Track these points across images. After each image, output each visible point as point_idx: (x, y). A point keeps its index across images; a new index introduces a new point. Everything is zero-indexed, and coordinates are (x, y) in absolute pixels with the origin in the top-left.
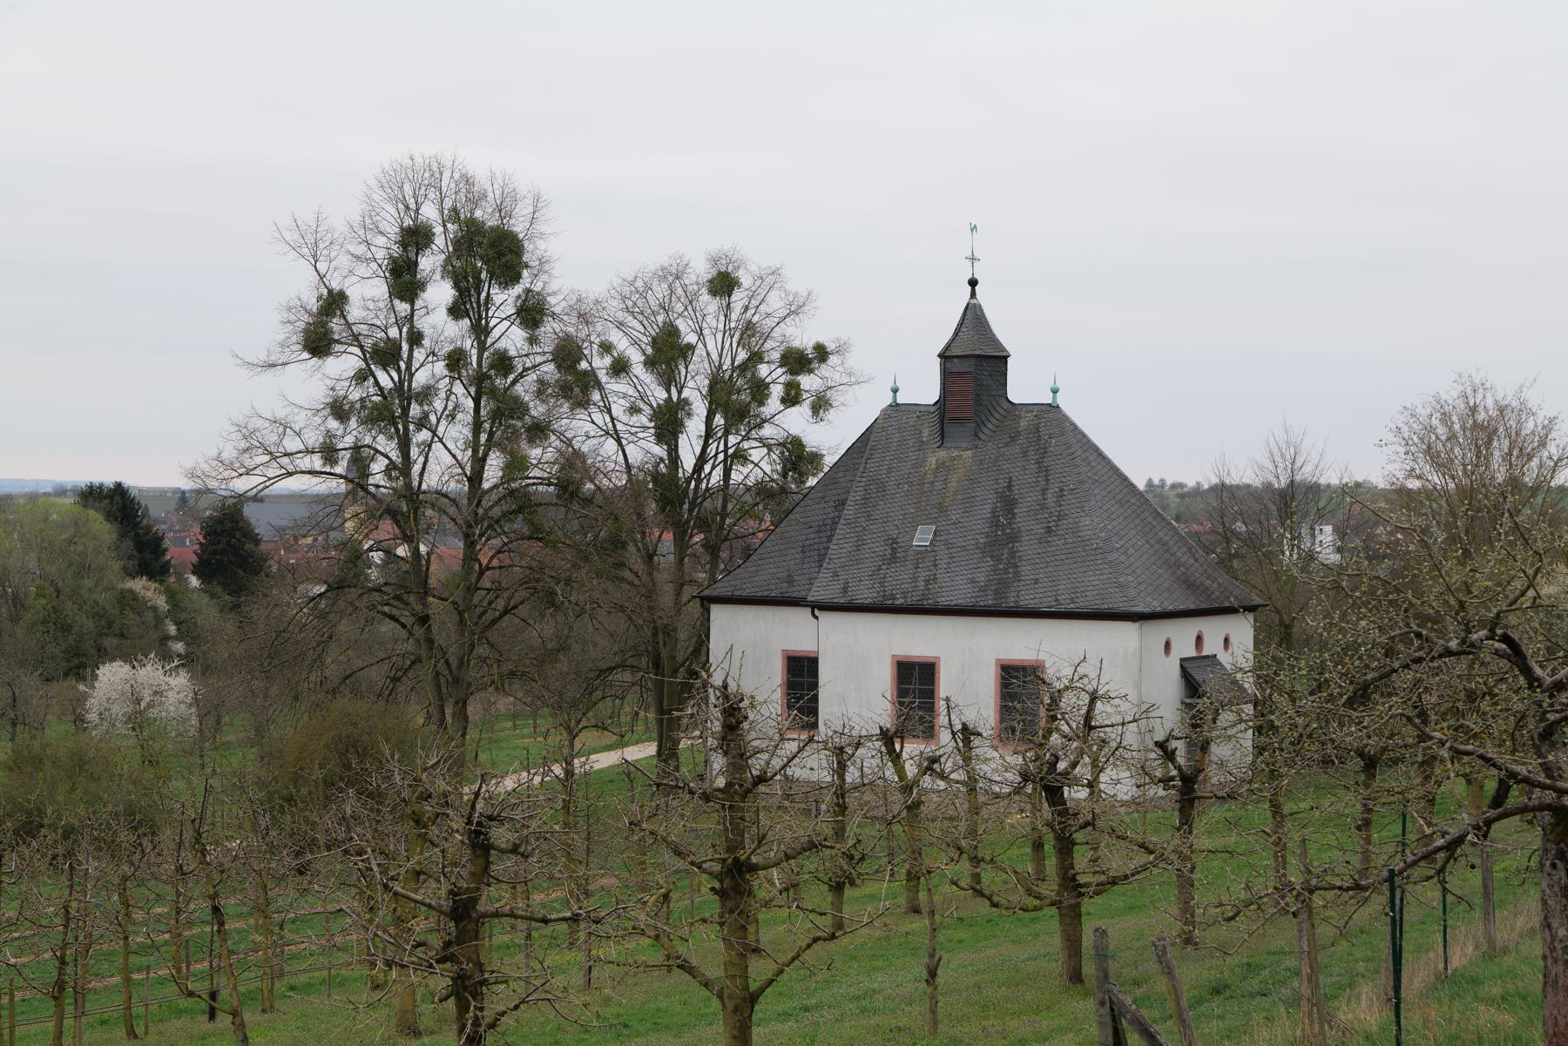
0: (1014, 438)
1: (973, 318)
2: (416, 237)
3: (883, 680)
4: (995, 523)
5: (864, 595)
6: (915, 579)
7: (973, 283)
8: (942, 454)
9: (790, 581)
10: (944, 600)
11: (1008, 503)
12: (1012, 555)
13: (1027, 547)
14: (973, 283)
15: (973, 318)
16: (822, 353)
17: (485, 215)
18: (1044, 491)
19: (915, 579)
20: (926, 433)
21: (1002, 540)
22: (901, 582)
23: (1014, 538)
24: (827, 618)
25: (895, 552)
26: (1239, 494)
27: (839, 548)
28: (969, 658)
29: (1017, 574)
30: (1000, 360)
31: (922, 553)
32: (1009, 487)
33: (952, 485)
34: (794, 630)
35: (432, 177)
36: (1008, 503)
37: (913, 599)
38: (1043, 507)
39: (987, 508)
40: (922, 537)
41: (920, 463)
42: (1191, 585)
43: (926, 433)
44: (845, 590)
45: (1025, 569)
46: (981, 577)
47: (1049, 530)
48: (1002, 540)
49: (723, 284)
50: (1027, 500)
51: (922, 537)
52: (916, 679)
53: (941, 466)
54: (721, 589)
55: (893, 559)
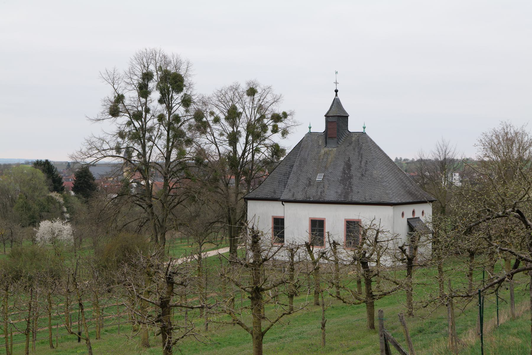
0: (350, 144)
1: (336, 103)
2: (147, 76)
3: (306, 226)
4: (344, 172)
5: (300, 197)
6: (317, 192)
7: (336, 91)
8: (326, 149)
9: (275, 193)
10: (327, 199)
11: (348, 166)
12: (350, 183)
13: (355, 181)
14: (336, 91)
15: (336, 103)
16: (285, 115)
18: (361, 162)
19: (317, 192)
20: (320, 142)
21: (346, 179)
22: (312, 193)
23: (351, 177)
24: (287, 205)
25: (310, 183)
27: (291, 181)
28: (335, 219)
29: (352, 190)
30: (345, 117)
31: (319, 183)
32: (349, 160)
33: (329, 160)
35: (152, 56)
36: (348, 166)
37: (316, 199)
38: (360, 167)
40: (319, 178)
41: (318, 152)
42: (410, 193)
43: (320, 142)
44: (293, 195)
45: (354, 188)
46: (339, 191)
47: (362, 175)
48: (346, 179)
49: (252, 92)
50: (355, 165)
51: (319, 178)
53: (326, 153)
54: (251, 195)
55: (309, 185)
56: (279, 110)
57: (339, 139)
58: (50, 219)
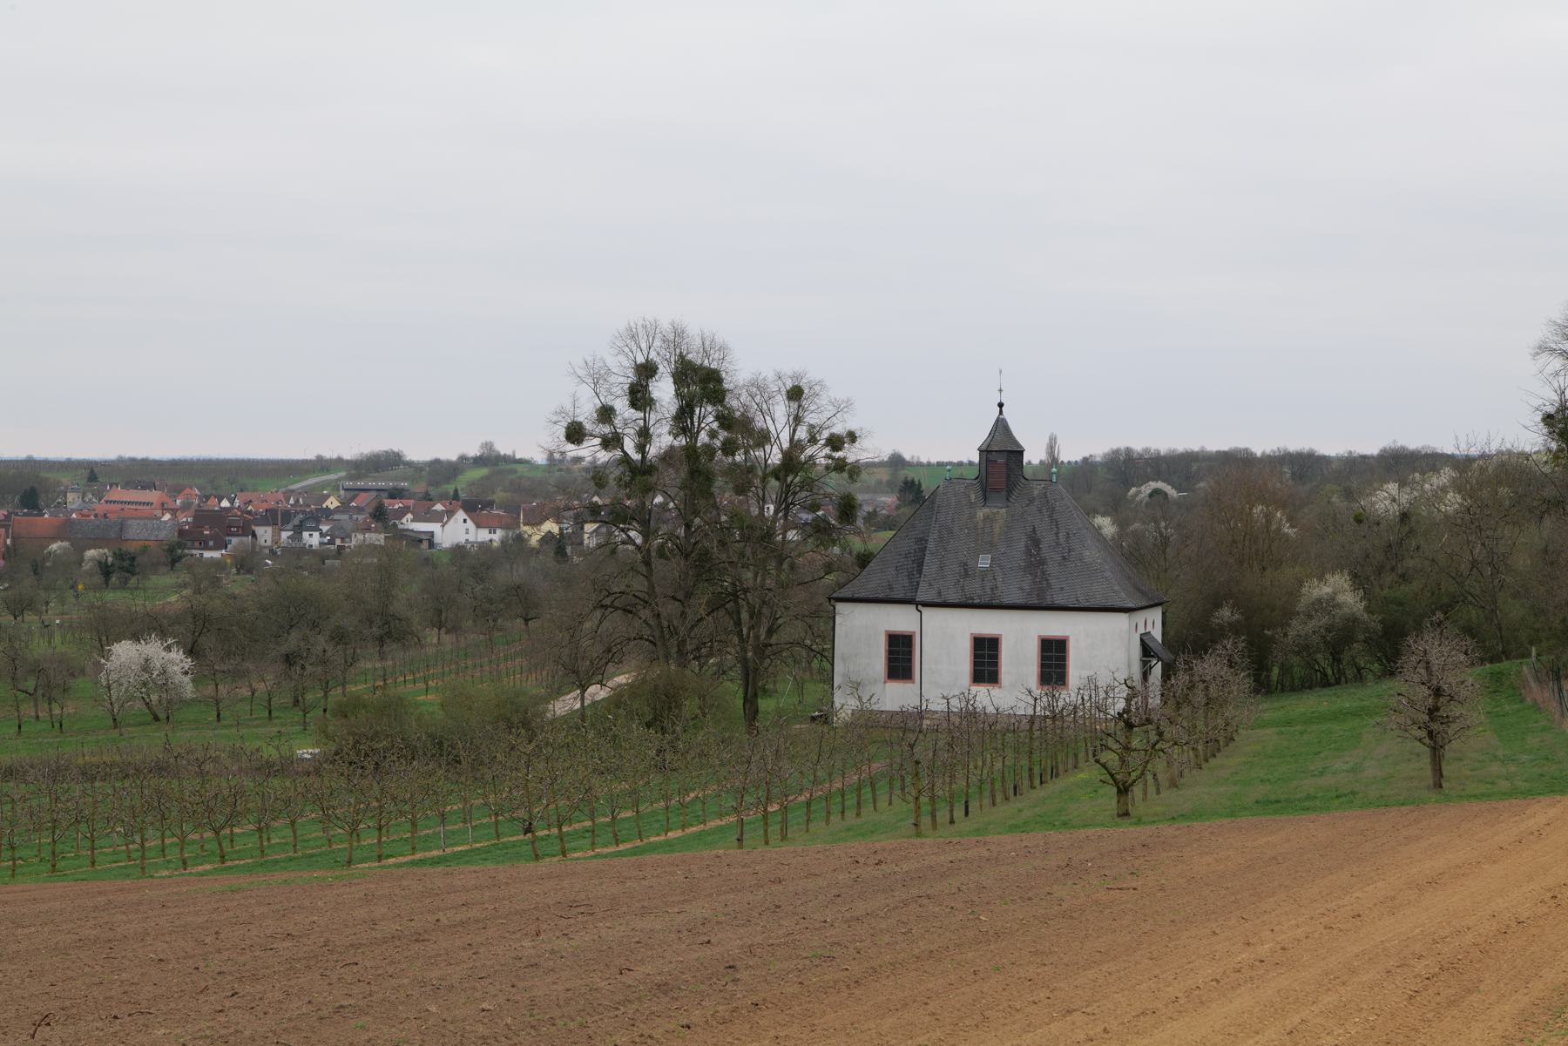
0: (1031, 501)
1: (1001, 427)
2: (647, 371)
4: (1028, 552)
5: (953, 597)
6: (983, 588)
7: (1001, 405)
8: (986, 510)
9: (891, 588)
11: (1034, 541)
12: (1043, 573)
13: (1052, 568)
14: (1001, 405)
15: (1001, 427)
16: (852, 437)
17: (694, 357)
18: (1057, 534)
19: (983, 588)
20: (973, 497)
21: (1035, 563)
22: (974, 589)
23: (1043, 562)
24: (927, 612)
25: (966, 571)
26: (928, 486)
27: (930, 567)
28: (1020, 636)
29: (1049, 586)
30: (1020, 453)
31: (984, 572)
32: (1034, 531)
33: (997, 530)
34: (901, 619)
35: (651, 330)
36: (1034, 541)
37: (985, 600)
38: (1058, 544)
39: (1023, 544)
40: (984, 562)
41: (972, 516)
42: (1143, 593)
43: (973, 497)
44: (939, 594)
45: (1053, 581)
46: (1026, 586)
48: (1035, 563)
49: (795, 394)
50: (1047, 541)
51: (984, 562)
52: (1053, 655)
54: (845, 593)
55: (966, 574)
56: (839, 429)
57: (1009, 492)
58: (136, 637)
